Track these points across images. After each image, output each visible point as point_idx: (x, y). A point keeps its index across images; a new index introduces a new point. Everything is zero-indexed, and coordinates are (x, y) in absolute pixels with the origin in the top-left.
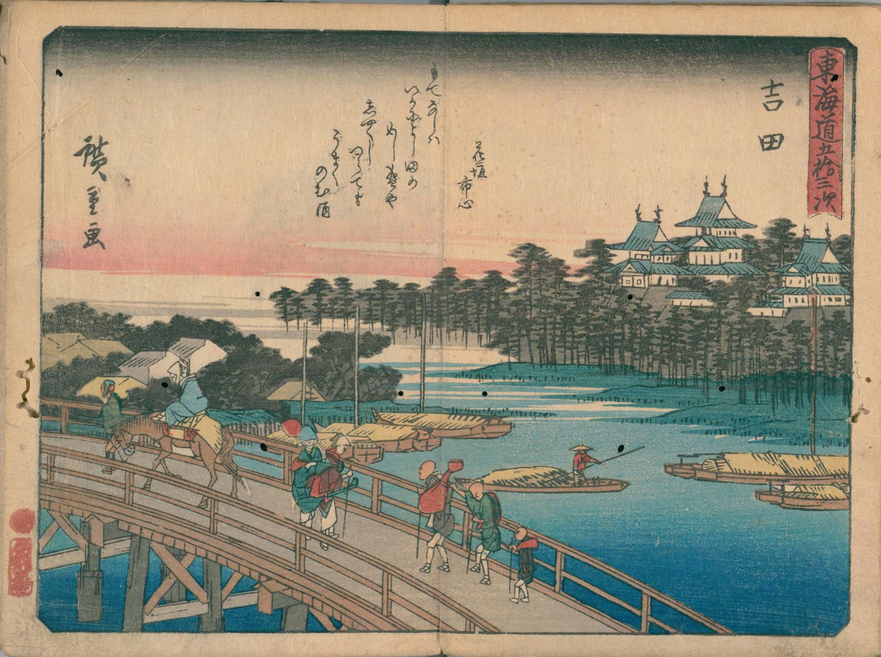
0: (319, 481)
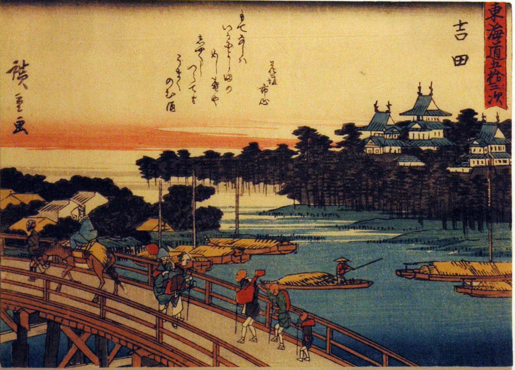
0: (175, 284)
